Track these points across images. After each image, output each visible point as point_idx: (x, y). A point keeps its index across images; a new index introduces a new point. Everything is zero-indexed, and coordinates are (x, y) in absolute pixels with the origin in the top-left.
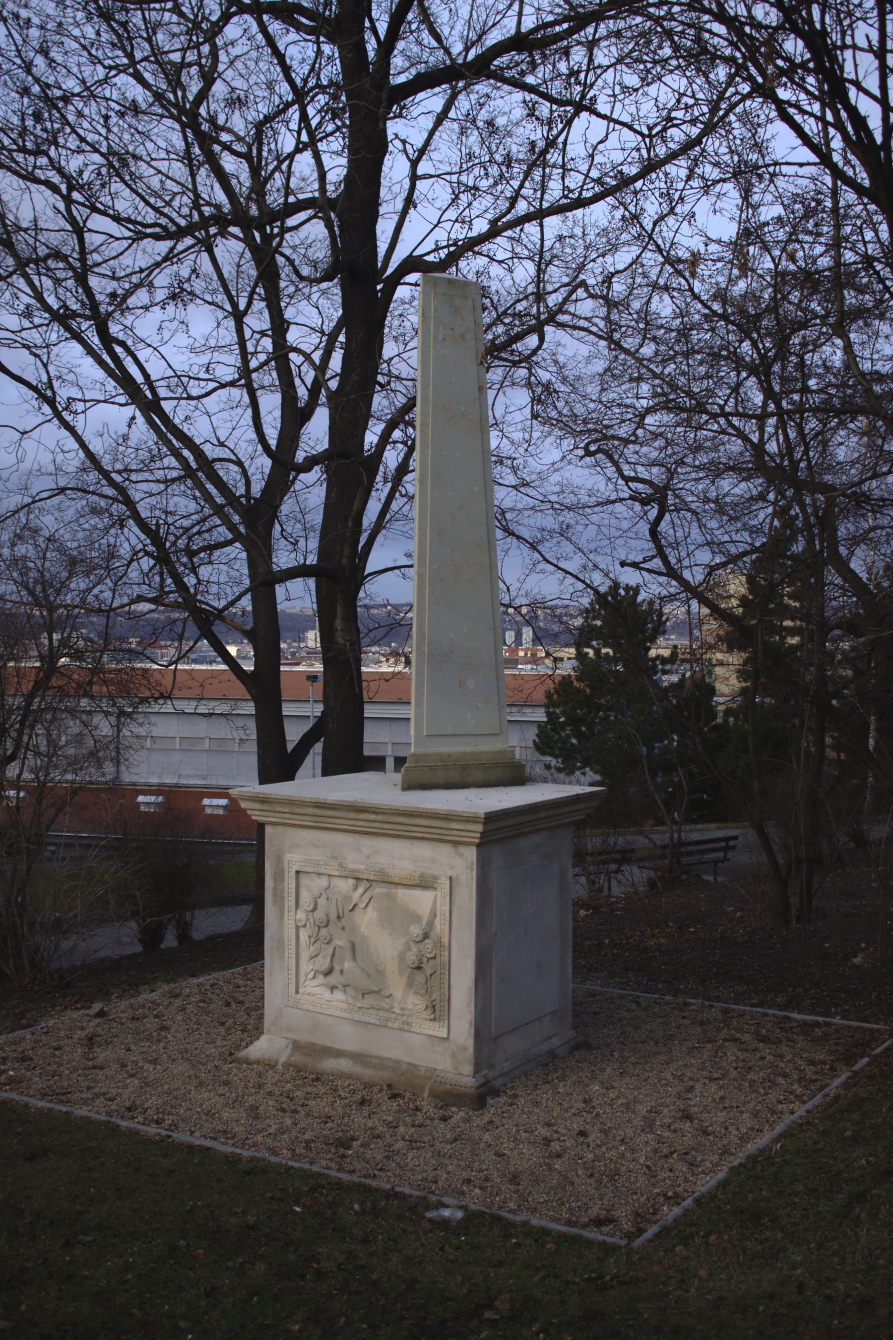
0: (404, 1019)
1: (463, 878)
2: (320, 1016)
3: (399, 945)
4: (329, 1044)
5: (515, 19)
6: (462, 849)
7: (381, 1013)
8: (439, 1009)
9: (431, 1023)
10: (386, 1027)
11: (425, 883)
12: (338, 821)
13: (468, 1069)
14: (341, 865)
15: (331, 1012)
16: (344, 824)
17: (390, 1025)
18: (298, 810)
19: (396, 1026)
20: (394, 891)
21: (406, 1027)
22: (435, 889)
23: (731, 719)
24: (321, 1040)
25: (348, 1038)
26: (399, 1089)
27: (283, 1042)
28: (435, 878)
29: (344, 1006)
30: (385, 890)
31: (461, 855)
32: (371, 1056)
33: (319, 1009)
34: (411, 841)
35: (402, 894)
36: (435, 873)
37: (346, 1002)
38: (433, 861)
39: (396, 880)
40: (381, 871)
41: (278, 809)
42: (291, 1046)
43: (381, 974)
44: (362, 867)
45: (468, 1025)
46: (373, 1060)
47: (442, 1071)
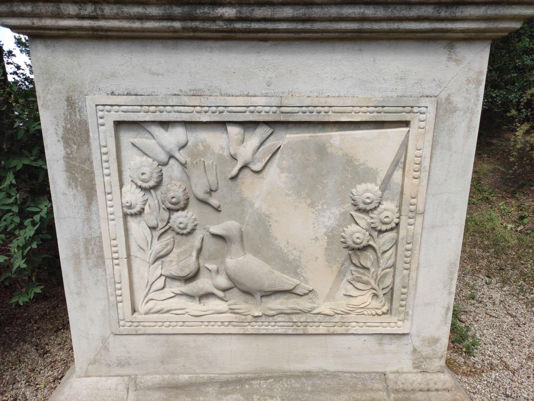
1: (458, 100)
3: (330, 216)
7: (295, 318)
17: (310, 330)
22: (406, 124)
35: (336, 138)
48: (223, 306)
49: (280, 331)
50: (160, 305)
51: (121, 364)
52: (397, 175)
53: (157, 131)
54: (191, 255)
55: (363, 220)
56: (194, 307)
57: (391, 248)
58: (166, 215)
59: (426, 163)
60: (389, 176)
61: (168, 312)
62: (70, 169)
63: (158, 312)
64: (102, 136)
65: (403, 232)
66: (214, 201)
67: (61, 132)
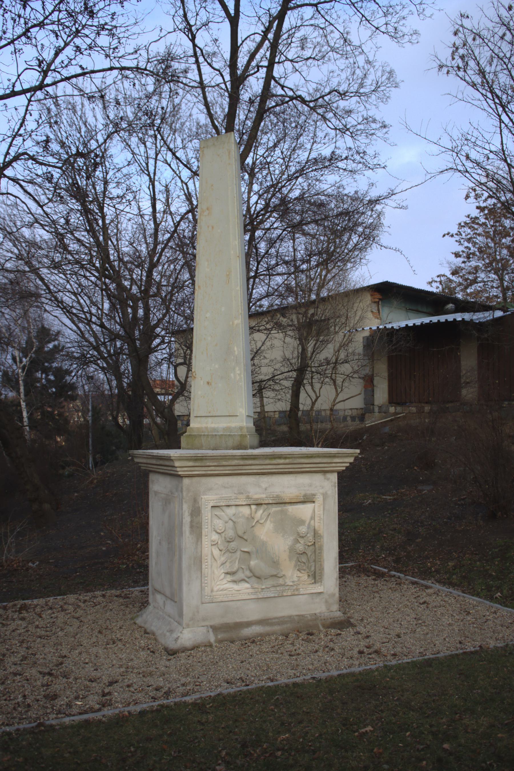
0: (295, 587)
1: (329, 493)
2: (231, 603)
3: (290, 541)
4: (238, 620)
5: (241, 35)
6: (329, 475)
7: (278, 589)
8: (316, 577)
9: (313, 585)
10: (283, 596)
11: (308, 500)
12: (253, 467)
13: (335, 607)
14: (248, 497)
15: (240, 597)
16: (255, 469)
17: (285, 594)
18: (224, 463)
19: (289, 594)
20: (285, 508)
21: (296, 593)
22: (314, 502)
23: (130, 458)
24: (231, 619)
25: (253, 612)
26: (305, 630)
27: (204, 630)
28: (314, 495)
29: (251, 591)
30: (279, 509)
31: (328, 479)
32: (271, 619)
33: (230, 598)
34: (296, 475)
35: (290, 508)
36: (313, 492)
37: (253, 588)
38: (310, 485)
39: (288, 501)
40: (278, 496)
41: (208, 464)
42: (211, 630)
43: (275, 563)
44: (264, 496)
45: (335, 580)
46: (274, 621)
47: (320, 613)
48: (247, 585)
49: (272, 595)
50: (222, 587)
51: (204, 620)
52: (312, 522)
53: (225, 508)
54: (235, 562)
55: (302, 541)
56: (236, 587)
57: (502, 137)
58: (227, 544)
59: (322, 517)
60: (310, 523)
61: (225, 590)
62: (192, 527)
63: (221, 591)
64: (207, 514)
65: (317, 546)
66: (245, 537)
67: (190, 512)
